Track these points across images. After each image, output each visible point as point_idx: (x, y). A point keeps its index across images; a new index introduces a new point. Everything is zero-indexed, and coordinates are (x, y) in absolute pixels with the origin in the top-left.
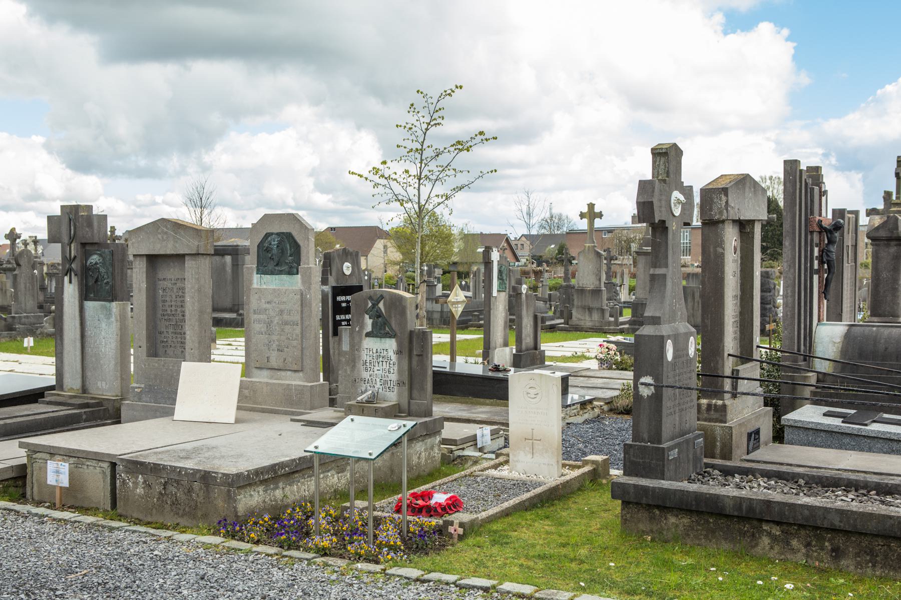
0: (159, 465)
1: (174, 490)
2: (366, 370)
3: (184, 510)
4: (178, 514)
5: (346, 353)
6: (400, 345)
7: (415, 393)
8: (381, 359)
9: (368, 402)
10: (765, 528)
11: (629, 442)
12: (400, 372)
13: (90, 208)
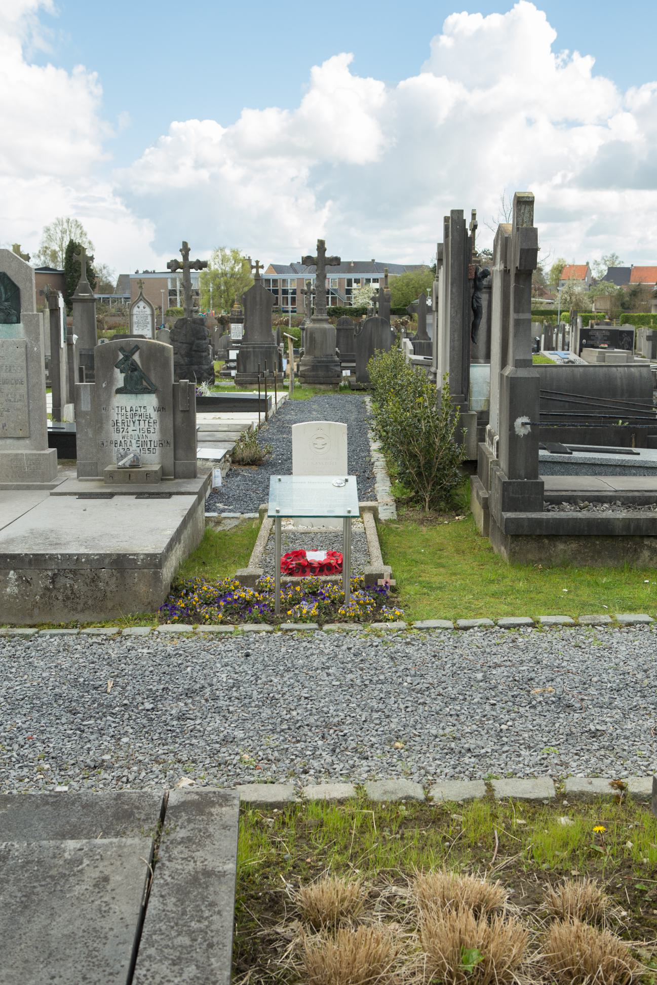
0: (43, 555)
1: (68, 582)
2: (118, 431)
3: (86, 603)
4: (75, 610)
5: (86, 413)
6: (162, 400)
7: (181, 452)
8: (137, 418)
9: (132, 466)
10: (646, 543)
11: (507, 480)
12: (163, 430)
13: (439, 245)
